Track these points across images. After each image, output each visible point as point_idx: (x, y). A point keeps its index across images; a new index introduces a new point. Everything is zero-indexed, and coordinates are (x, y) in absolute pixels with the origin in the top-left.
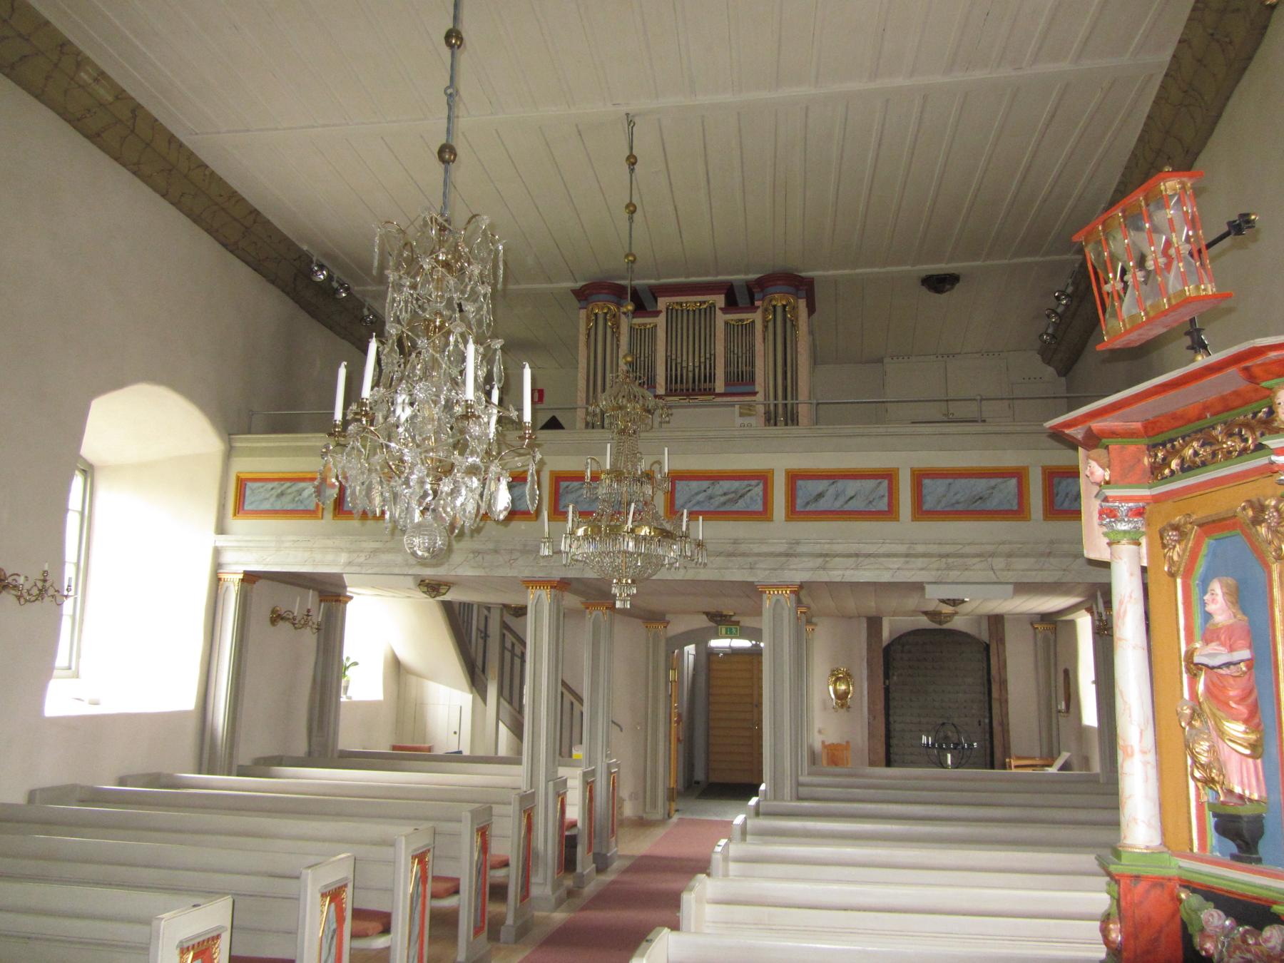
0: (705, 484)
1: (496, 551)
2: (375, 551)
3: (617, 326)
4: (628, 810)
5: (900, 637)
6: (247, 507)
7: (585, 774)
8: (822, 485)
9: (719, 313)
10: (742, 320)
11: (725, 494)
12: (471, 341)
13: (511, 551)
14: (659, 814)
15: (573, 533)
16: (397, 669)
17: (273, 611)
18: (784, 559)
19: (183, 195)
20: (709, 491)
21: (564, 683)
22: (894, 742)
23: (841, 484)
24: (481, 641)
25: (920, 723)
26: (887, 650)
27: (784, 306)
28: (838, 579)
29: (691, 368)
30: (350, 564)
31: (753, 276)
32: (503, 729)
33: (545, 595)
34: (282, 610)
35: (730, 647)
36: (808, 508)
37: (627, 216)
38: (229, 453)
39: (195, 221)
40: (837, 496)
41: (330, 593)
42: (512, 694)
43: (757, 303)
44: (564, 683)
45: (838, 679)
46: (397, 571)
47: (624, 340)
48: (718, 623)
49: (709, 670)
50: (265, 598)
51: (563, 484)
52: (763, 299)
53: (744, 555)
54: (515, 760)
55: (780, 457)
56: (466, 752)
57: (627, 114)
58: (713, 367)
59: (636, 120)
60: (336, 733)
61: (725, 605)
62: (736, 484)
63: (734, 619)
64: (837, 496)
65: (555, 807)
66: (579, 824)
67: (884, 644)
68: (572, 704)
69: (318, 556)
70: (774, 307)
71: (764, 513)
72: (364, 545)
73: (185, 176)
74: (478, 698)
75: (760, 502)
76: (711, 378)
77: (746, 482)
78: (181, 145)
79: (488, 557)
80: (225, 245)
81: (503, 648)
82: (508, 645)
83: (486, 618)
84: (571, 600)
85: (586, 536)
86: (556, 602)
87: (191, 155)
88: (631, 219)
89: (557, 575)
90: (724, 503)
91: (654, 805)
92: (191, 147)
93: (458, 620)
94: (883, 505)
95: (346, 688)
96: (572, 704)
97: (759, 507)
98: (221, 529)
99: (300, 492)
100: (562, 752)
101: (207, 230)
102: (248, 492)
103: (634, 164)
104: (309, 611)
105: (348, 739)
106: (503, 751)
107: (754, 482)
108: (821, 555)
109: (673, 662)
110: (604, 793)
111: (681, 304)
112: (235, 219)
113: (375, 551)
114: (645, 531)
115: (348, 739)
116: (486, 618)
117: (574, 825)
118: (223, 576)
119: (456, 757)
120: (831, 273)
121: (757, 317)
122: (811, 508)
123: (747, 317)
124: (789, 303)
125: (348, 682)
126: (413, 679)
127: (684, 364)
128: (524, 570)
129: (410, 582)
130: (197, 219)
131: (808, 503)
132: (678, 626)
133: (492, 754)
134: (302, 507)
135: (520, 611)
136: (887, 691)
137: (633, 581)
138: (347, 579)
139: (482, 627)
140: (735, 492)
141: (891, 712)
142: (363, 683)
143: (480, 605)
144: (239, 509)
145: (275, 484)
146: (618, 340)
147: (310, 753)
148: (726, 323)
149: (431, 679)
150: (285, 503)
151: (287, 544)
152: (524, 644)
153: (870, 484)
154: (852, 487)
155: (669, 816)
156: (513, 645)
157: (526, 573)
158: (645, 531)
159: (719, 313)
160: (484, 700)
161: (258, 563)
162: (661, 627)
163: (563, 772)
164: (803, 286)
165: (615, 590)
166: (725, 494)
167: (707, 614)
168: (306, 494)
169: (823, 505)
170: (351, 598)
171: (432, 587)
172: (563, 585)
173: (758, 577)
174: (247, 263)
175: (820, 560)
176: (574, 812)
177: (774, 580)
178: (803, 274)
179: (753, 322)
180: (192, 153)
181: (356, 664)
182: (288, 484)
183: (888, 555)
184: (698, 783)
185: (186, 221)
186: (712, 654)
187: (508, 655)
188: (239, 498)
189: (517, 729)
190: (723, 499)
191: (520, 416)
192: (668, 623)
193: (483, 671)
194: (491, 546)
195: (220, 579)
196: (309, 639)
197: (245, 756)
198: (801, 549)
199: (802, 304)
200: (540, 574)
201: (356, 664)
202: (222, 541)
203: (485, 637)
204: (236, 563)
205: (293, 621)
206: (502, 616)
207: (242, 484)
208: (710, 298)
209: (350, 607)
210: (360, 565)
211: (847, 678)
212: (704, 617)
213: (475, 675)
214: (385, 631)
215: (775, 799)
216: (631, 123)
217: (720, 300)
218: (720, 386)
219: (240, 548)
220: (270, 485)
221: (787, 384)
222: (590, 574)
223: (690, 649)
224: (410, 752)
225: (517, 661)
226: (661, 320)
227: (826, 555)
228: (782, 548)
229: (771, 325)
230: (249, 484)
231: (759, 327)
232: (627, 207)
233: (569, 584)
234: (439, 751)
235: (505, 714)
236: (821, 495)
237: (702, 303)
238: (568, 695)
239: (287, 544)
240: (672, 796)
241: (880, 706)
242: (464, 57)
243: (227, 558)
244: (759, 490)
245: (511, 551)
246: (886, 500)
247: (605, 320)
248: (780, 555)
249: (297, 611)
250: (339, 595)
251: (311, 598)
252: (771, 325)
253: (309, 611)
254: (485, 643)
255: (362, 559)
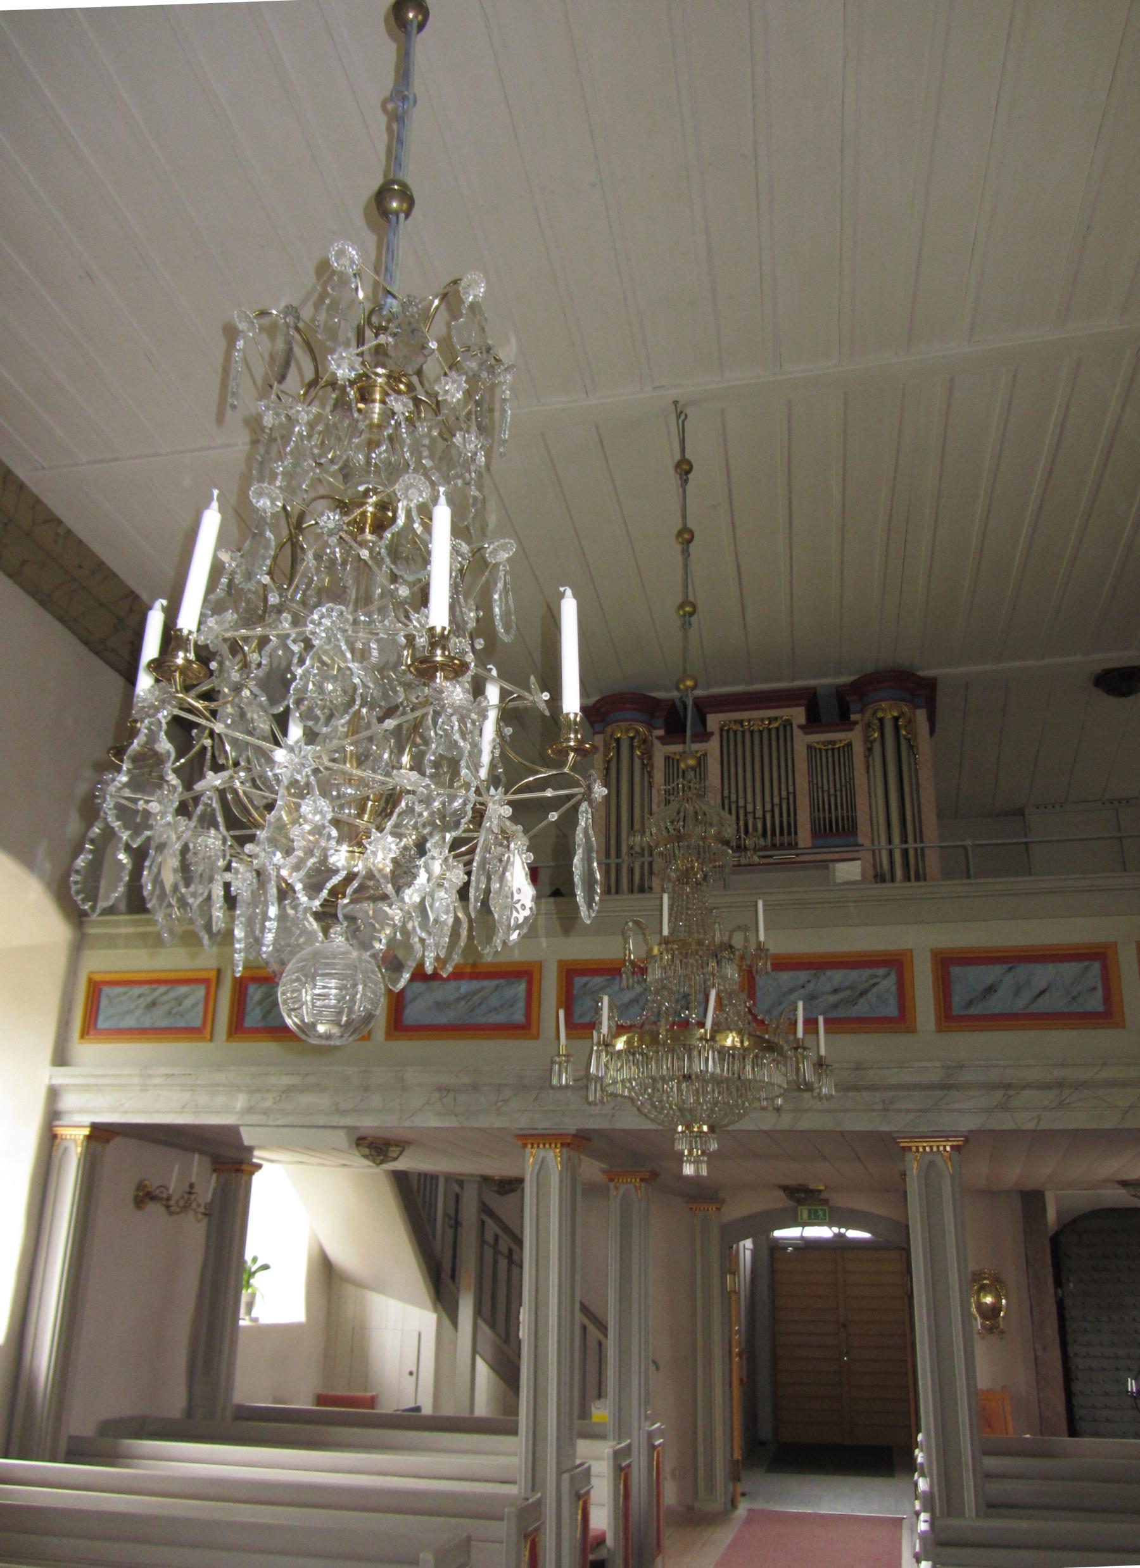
0: (803, 976)
1: (475, 1088)
2: (289, 1090)
3: (648, 754)
4: (670, 1495)
5: (1074, 1221)
6: (102, 1024)
7: (617, 1455)
8: (992, 973)
9: (797, 733)
10: (833, 742)
11: (836, 991)
12: (442, 499)
13: (499, 1088)
14: (718, 1503)
15: (608, 1045)
16: (327, 1276)
17: (140, 1186)
18: (938, 1093)
19: (24, 563)
20: (810, 987)
21: (584, 1309)
22: (1077, 1387)
23: (1022, 970)
24: (450, 1233)
25: (1116, 1357)
26: (1055, 1240)
27: (896, 719)
28: (1031, 1126)
29: (759, 814)
30: (250, 1110)
31: (845, 679)
32: (482, 1367)
33: (554, 1158)
34: (153, 1183)
35: (802, 1238)
36: (973, 1011)
37: (678, 548)
38: (78, 947)
39: (42, 603)
40: (1018, 991)
41: (226, 1161)
42: (499, 1314)
43: (853, 717)
44: (584, 1309)
45: (983, 1288)
46: (322, 1121)
47: (659, 776)
48: (800, 1202)
49: (773, 1272)
50: (127, 1168)
51: (579, 981)
52: (862, 711)
53: (873, 1088)
54: (501, 1424)
55: (918, 936)
56: (427, 1410)
57: (676, 403)
58: (792, 812)
59: (689, 411)
60: (230, 1378)
61: (815, 1174)
62: (854, 975)
63: (823, 1196)
64: (1018, 991)
65: (573, 1519)
66: (610, 1541)
67: (1051, 1234)
68: (584, 1328)
69: (203, 1099)
70: (881, 720)
71: (901, 1020)
72: (273, 1080)
73: (28, 535)
74: (446, 1321)
75: (893, 1001)
76: (791, 828)
77: (868, 972)
78: (22, 487)
79: (462, 1098)
80: (86, 643)
81: (482, 1242)
82: (489, 1238)
83: (457, 1196)
84: (591, 1169)
85: (630, 1050)
86: (571, 1171)
87: (37, 503)
88: (686, 553)
89: (571, 1125)
90: (835, 1006)
91: (711, 1488)
92: (36, 490)
93: (416, 1199)
94: (1095, 1003)
95: (250, 1306)
96: (584, 1328)
97: (892, 1011)
98: (61, 1058)
99: (179, 1001)
100: (578, 1423)
101: (61, 620)
102: (104, 1001)
103: (688, 472)
104: (192, 1186)
105: (251, 1386)
106: (482, 1408)
107: (881, 971)
108: (995, 1087)
109: (730, 1263)
110: (644, 1486)
111: (741, 723)
112: (101, 604)
113: (289, 1090)
114: (730, 1040)
115: (251, 1386)
116: (457, 1196)
117: (600, 1541)
118: (60, 1131)
119: (411, 1421)
120: (962, 670)
121: (855, 737)
122: (976, 1010)
123: (840, 737)
124: (902, 714)
125: (253, 1295)
126: (350, 1289)
127: (750, 808)
128: (523, 1115)
129: (341, 1138)
130: (45, 601)
131: (970, 1003)
132: (736, 1209)
133: (465, 1414)
134: (182, 1024)
135: (511, 1186)
136: (1060, 1305)
137: (712, 1129)
138: (248, 1137)
139: (452, 1212)
140: (851, 988)
141: (1070, 1340)
142: (277, 1297)
143: (451, 1178)
144: (90, 1028)
145: (145, 989)
146: (650, 777)
147: (189, 1412)
148: (810, 747)
149: (381, 1289)
150: (158, 1018)
151: (157, 1081)
152: (520, 1242)
153: (1071, 969)
154: (1042, 974)
155: (734, 1505)
156: (496, 1237)
157: (523, 1122)
158: (730, 1040)
159: (797, 733)
160: (455, 1323)
161: (113, 1110)
162: (712, 1209)
163: (584, 1448)
164: (917, 688)
165: (682, 1147)
166: (836, 991)
167: (785, 1189)
168: (188, 1003)
169: (997, 1003)
170: (259, 1166)
171: (376, 1147)
172: (578, 1142)
173: (895, 1124)
174: (117, 670)
175: (999, 1094)
176: (601, 1519)
177: (923, 1129)
178: (920, 673)
179: (850, 745)
180: (38, 501)
181: (266, 1267)
182: (162, 989)
183: (1112, 1084)
184: (763, 1443)
185: (30, 602)
186: (777, 1247)
187: (489, 1252)
188: (90, 1012)
189: (507, 1371)
190: (832, 999)
191: (556, 700)
192: (723, 1202)
193: (453, 1277)
194: (465, 1080)
195: (55, 1137)
196: (194, 1232)
197: (81, 1422)
198: (968, 1076)
199: (921, 715)
200: (544, 1124)
201: (266, 1267)
202: (62, 1077)
203: (456, 1224)
204: (81, 1111)
205: (166, 1202)
206: (480, 1193)
207: (95, 989)
208: (784, 713)
209: (257, 1179)
210: (265, 1112)
211: (997, 1285)
212: (781, 1193)
213: (441, 1285)
214: (302, 1220)
215: (949, 1515)
216: (681, 415)
217: (798, 715)
218: (804, 836)
219: (86, 1088)
220: (136, 991)
221: (908, 825)
222: (630, 1121)
223: (748, 1243)
224: (343, 1410)
225: (503, 1263)
226: (713, 746)
227: (1008, 1086)
228: (935, 1077)
229: (877, 747)
230: (107, 991)
231: (858, 749)
232: (680, 534)
233: (588, 1139)
234: (388, 1406)
235: (485, 1345)
236: (991, 990)
237: (771, 720)
238: (588, 1323)
239: (157, 1081)
240: (735, 1477)
241: (1051, 1330)
242: (424, 44)
243: (68, 1102)
244: (889, 984)
245: (499, 1088)
246: (1099, 993)
247: (632, 747)
248: (930, 1087)
249: (174, 1185)
250: (241, 1162)
251: (198, 1168)
252: (877, 747)
253: (192, 1186)
254: (457, 1235)
255: (268, 1103)
